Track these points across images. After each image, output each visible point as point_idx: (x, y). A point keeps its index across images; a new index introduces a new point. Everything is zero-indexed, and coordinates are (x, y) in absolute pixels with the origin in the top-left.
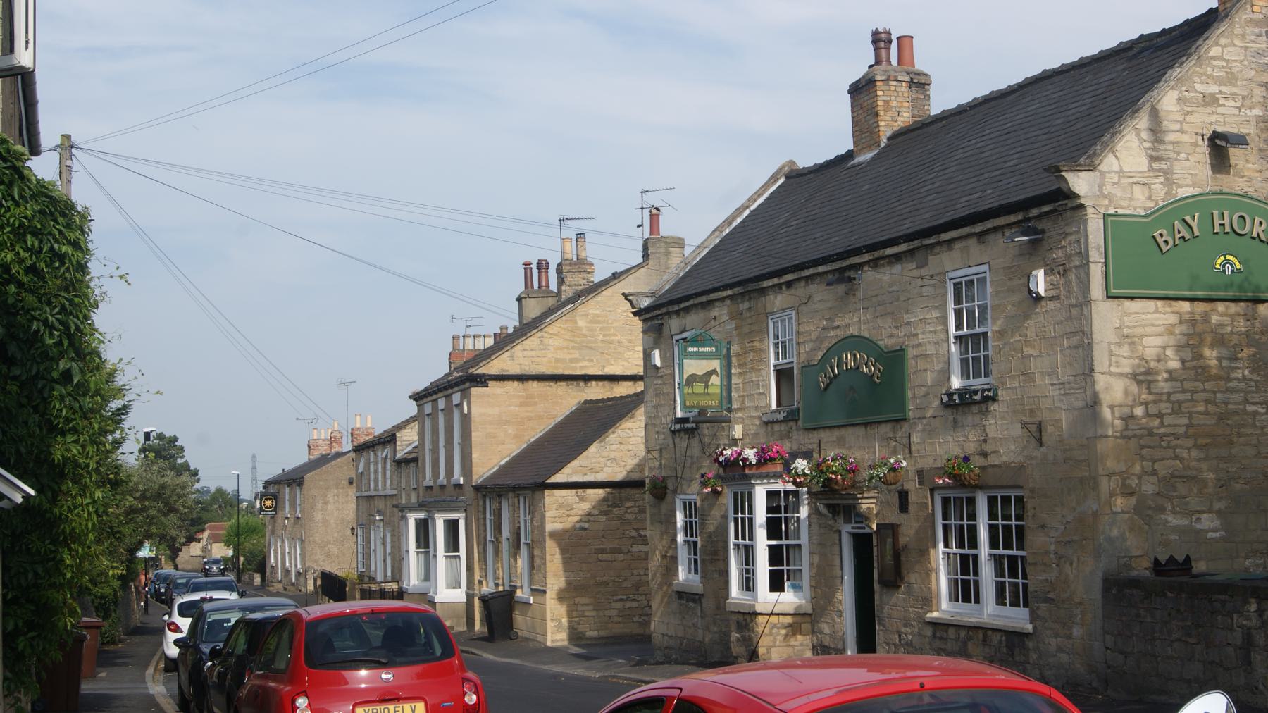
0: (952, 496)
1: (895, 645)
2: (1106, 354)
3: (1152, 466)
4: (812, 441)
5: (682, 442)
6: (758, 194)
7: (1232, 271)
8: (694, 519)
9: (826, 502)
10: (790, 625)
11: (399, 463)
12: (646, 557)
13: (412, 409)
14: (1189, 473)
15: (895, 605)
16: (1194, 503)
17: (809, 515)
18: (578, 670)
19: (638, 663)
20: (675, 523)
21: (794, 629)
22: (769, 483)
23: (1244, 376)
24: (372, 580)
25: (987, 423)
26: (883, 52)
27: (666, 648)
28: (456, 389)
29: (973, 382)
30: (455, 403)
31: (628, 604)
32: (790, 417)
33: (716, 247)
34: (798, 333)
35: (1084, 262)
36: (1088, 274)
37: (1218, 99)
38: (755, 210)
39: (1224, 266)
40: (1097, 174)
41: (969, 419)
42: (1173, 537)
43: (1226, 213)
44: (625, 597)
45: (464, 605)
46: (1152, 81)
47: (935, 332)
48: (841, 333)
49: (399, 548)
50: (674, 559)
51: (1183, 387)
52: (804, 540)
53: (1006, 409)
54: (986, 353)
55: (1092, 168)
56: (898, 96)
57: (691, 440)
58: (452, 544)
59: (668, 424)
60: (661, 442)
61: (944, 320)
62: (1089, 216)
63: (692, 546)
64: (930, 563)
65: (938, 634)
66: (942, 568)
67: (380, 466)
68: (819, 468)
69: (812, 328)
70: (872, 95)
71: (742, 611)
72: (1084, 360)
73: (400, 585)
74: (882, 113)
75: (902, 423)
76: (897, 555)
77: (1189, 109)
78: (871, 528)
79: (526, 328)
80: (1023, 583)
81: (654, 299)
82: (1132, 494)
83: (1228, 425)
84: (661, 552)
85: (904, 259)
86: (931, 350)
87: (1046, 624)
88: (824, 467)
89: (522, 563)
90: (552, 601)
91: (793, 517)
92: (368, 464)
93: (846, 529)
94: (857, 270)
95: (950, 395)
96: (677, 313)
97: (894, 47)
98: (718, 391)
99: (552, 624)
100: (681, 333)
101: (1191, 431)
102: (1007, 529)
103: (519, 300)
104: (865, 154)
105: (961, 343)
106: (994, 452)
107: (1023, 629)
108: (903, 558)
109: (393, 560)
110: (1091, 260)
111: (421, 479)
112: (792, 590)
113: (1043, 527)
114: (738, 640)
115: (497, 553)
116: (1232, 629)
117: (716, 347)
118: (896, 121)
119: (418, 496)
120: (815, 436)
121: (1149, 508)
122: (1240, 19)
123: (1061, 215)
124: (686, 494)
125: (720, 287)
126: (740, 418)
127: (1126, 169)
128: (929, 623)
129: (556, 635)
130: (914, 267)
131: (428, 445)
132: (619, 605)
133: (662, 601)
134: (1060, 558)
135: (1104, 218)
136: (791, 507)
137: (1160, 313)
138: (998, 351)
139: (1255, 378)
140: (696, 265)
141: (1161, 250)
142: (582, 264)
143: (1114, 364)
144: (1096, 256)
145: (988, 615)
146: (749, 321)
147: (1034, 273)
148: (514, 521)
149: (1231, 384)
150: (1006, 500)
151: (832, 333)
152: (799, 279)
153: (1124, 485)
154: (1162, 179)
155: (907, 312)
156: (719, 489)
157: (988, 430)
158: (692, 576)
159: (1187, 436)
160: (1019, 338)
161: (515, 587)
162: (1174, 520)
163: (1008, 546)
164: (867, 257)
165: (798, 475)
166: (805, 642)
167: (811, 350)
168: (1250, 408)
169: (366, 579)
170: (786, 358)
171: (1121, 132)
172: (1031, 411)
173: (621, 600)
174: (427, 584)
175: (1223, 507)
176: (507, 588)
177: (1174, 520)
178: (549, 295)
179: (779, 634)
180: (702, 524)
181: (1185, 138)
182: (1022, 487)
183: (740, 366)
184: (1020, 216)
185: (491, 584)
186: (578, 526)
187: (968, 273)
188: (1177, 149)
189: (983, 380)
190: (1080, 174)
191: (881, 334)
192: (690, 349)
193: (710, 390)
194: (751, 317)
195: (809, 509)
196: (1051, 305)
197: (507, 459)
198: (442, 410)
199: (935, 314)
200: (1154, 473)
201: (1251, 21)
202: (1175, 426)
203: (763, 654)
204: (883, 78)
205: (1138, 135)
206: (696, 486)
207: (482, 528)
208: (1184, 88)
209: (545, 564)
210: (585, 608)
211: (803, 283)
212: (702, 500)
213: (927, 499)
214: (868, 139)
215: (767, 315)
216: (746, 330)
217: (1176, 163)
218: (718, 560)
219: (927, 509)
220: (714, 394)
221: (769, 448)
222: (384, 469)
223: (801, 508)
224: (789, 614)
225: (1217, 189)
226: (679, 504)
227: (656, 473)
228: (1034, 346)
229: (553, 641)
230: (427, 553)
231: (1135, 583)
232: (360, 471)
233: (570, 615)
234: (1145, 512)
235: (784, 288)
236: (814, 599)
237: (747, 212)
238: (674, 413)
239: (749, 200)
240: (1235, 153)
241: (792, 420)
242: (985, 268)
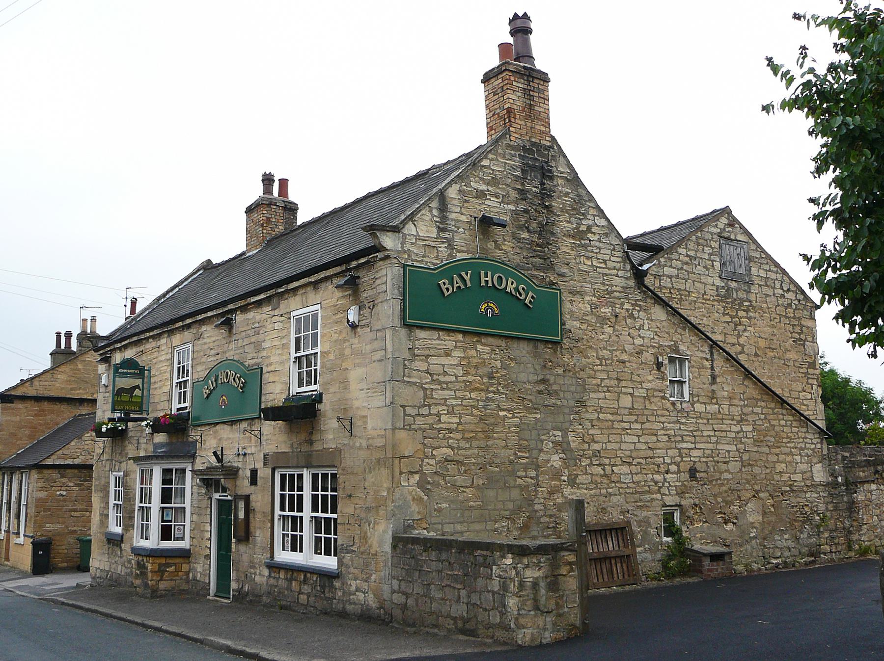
0: (287, 473)
3: (432, 453)
9: (200, 477)
43: (489, 273)
51: (455, 395)
54: (315, 368)
56: (276, 215)
65: (273, 575)
77: (466, 198)
80: (334, 538)
85: (264, 304)
96: (120, 349)
101: (460, 427)
118: (274, 231)
121: (429, 483)
122: (502, 143)
137: (442, 340)
150: (325, 476)
159: (457, 430)
181: (463, 218)
188: (458, 225)
189: (313, 387)
190: (388, 233)
202: (449, 423)
205: (431, 211)
208: (463, 184)
211: (197, 325)
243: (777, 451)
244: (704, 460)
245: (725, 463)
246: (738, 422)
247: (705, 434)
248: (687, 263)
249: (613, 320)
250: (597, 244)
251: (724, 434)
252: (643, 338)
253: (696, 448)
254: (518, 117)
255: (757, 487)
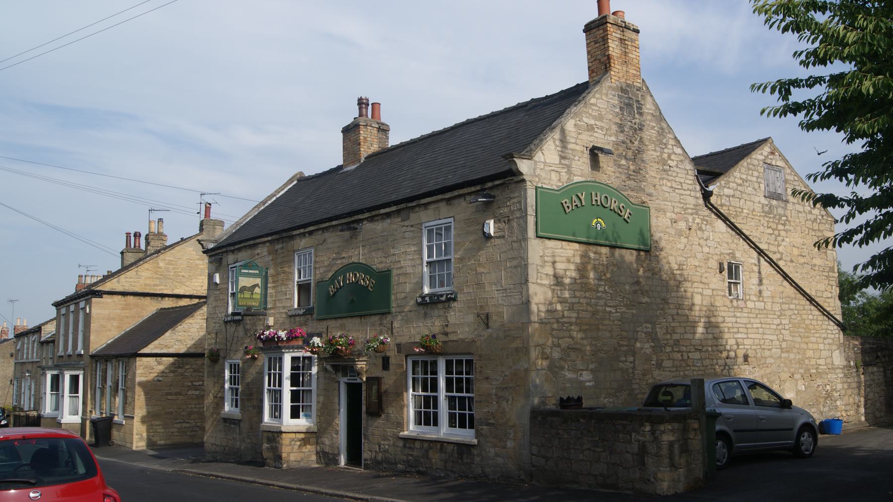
1: (376, 452)
2: (535, 272)
4: (322, 327)
5: (232, 329)
6: (281, 189)
7: (601, 228)
8: (237, 375)
10: (303, 439)
11: (42, 343)
12: (202, 397)
13: (53, 312)
14: (577, 346)
15: (377, 427)
16: (580, 365)
17: (318, 372)
18: (156, 466)
19: (194, 462)
20: (224, 377)
21: (305, 442)
22: (293, 352)
23: (605, 290)
24: (22, 410)
25: (449, 314)
26: (364, 110)
27: (214, 452)
28: (82, 299)
29: (438, 290)
30: (81, 307)
31: (184, 425)
32: (308, 313)
33: (255, 216)
34: (315, 262)
35: (523, 214)
36: (526, 222)
37: (594, 128)
38: (279, 197)
39: (596, 225)
40: (533, 162)
41: (436, 312)
42: (568, 385)
44: (182, 421)
45: (80, 425)
46: (560, 113)
47: (413, 260)
48: (345, 262)
49: (40, 392)
50: (222, 399)
52: (314, 387)
53: (463, 306)
55: (530, 158)
57: (238, 327)
58: (74, 388)
59: (222, 318)
60: (217, 328)
61: (420, 252)
62: (528, 187)
63: (234, 391)
64: (403, 401)
65: (407, 445)
66: (411, 404)
67: (30, 345)
68: (330, 342)
69: (325, 259)
70: (357, 133)
71: (272, 430)
72: (521, 275)
73: (39, 412)
74: (362, 144)
75: (387, 315)
76: (380, 396)
77: (580, 131)
78: (362, 379)
79: (125, 268)
81: (216, 244)
82: (547, 358)
83: (597, 318)
84: (213, 394)
86: (409, 270)
87: (488, 439)
88: (334, 342)
89: (119, 400)
90: (138, 423)
91: (307, 373)
92: (23, 344)
93: (343, 380)
94: (358, 224)
95: (423, 297)
96: (233, 251)
97: (370, 107)
98: (259, 297)
99: (137, 437)
100: (234, 263)
101: (578, 321)
102: (459, 381)
103: (122, 253)
104: (350, 166)
105: (430, 266)
106: (453, 332)
107: (470, 442)
108: (384, 398)
109: (35, 399)
110: (528, 213)
111: (56, 352)
112: (305, 418)
113: (487, 378)
114: (268, 448)
115: (103, 394)
116: (630, 442)
117: (259, 271)
119: (53, 362)
120: (324, 324)
123: (507, 186)
124: (232, 359)
125: (263, 235)
126: (272, 313)
127: (548, 161)
128: (401, 438)
129: (139, 443)
130: (400, 220)
131: (62, 332)
132: (178, 426)
133: (213, 423)
134: (499, 398)
135: (536, 189)
136: (306, 366)
137: (564, 249)
138: (458, 270)
139: (610, 292)
140: (243, 226)
141: (565, 212)
142: (160, 235)
143: (539, 278)
144: (531, 211)
145: (443, 433)
146: (282, 255)
147: (487, 222)
148: (115, 377)
149: (599, 294)
150: (459, 362)
151: (339, 262)
152: (317, 230)
153: (543, 353)
154: (566, 170)
155: (393, 248)
156: (256, 356)
157: (449, 319)
158: (234, 409)
159: (576, 324)
160: (474, 262)
161: (114, 415)
162: (569, 375)
163: (459, 390)
164: (367, 215)
165: (314, 347)
166: (311, 450)
167: (324, 272)
168: (608, 309)
169: (18, 409)
170: (305, 277)
171: (546, 139)
172: (481, 306)
173: (180, 422)
174: (56, 412)
175: (593, 367)
176: (108, 415)
177: (569, 375)
178: (140, 251)
179: (296, 445)
180: (242, 377)
182: (473, 354)
183: (274, 282)
184: (478, 188)
185: (98, 413)
186: (156, 379)
187: (439, 223)
188: (574, 153)
191: (374, 262)
192: (243, 271)
193: (254, 296)
194: (283, 253)
195: (318, 368)
196: (498, 241)
197: (112, 340)
198: (72, 312)
199: (413, 249)
200: (559, 346)
201: (610, 87)
203: (285, 457)
204: (364, 124)
205: (554, 142)
206: (240, 354)
207: (94, 380)
208: (578, 119)
209: (134, 401)
210: (158, 427)
211: (320, 232)
212: (244, 363)
213: (403, 361)
214: (353, 158)
215: (294, 251)
216: (279, 260)
217: (573, 162)
218: (253, 399)
219: (403, 367)
220: (256, 299)
221: (295, 331)
222: (33, 347)
223: (313, 368)
224: (303, 433)
225: (593, 179)
226: (227, 366)
227: (213, 346)
228: (485, 267)
229: (136, 447)
230: (57, 395)
231: (552, 413)
232: (18, 348)
233: (148, 431)
234: (554, 369)
235: (307, 235)
236: (319, 423)
237: (274, 199)
238: (227, 311)
239: (276, 191)
240: (602, 157)
241: (309, 314)
242: (452, 220)
243: (807, 340)
244: (753, 347)
245: (769, 350)
246: (779, 317)
247: (755, 326)
248: (740, 185)
249: (688, 231)
250: (675, 169)
251: (768, 326)
252: (709, 247)
253: (748, 338)
254: (616, 62)
255: (792, 370)
